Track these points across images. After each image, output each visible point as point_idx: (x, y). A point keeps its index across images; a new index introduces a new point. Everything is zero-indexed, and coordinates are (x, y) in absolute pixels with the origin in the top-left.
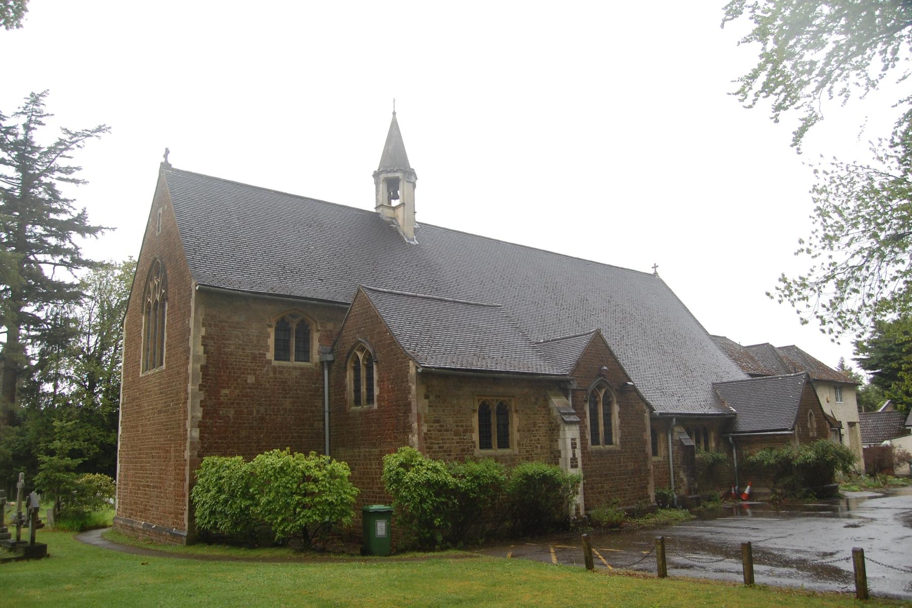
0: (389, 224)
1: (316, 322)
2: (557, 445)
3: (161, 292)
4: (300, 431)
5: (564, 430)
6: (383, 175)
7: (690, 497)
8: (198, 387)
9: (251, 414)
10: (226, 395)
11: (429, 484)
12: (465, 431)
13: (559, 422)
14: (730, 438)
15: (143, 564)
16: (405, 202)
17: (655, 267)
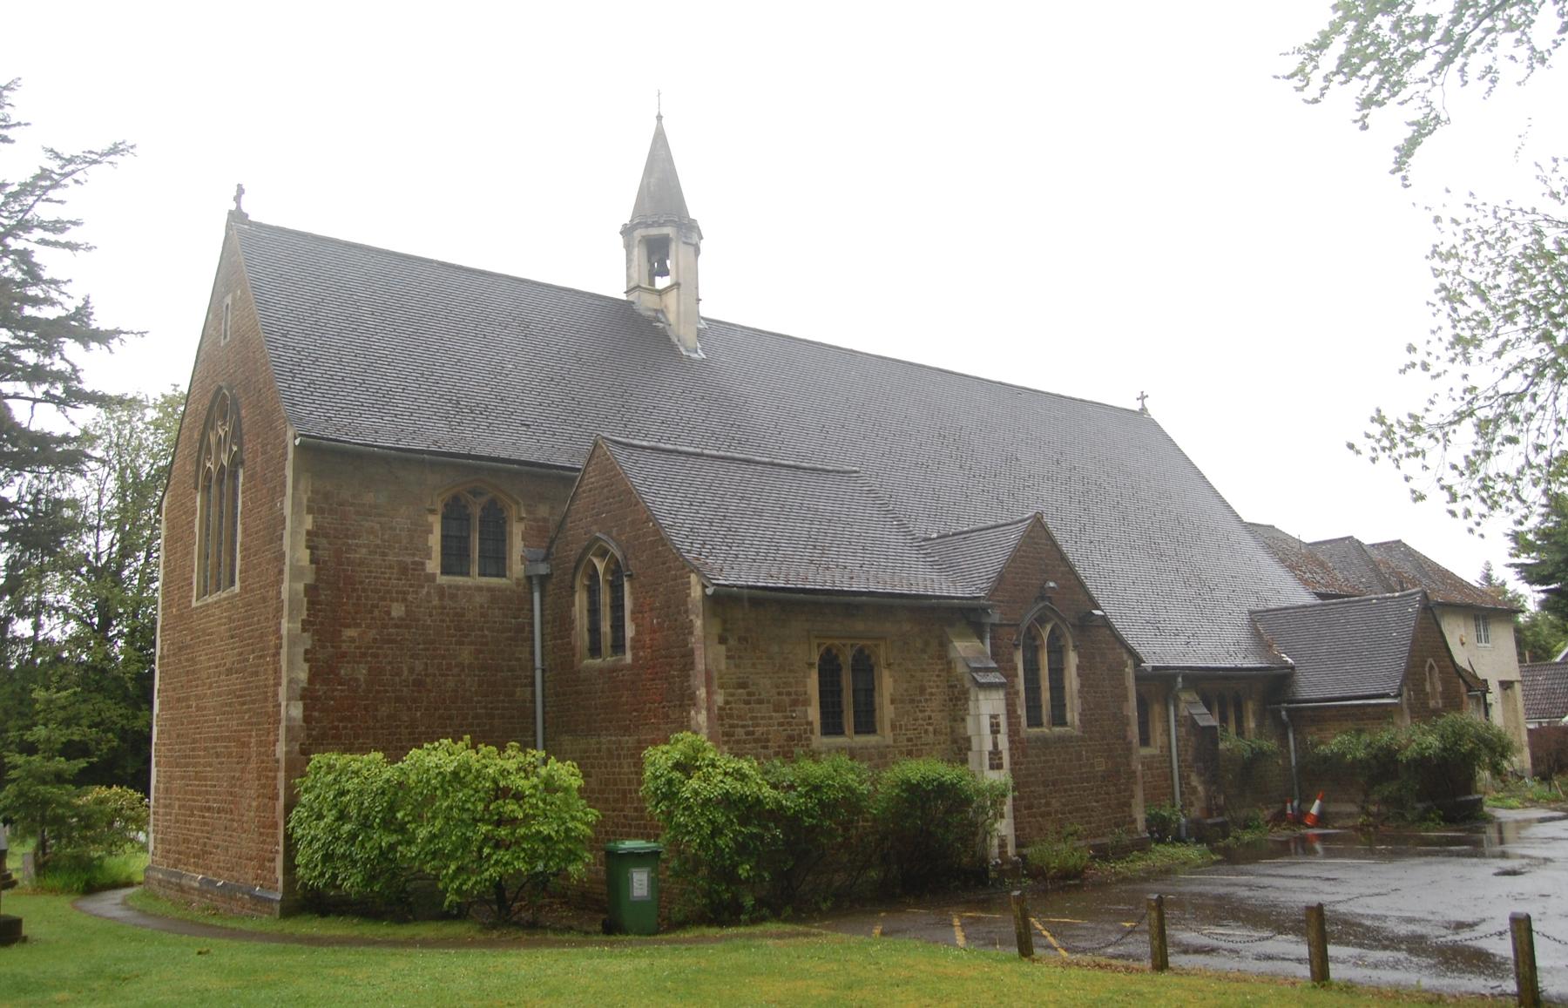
0: (651, 322)
1: (518, 503)
2: (965, 728)
3: (231, 449)
4: (490, 706)
5: (977, 700)
7: (1209, 821)
8: (300, 626)
9: (399, 674)
10: (353, 640)
12: (795, 703)
13: (968, 685)
14: (1284, 713)
15: (200, 953)
16: (681, 281)
17: (1143, 397)
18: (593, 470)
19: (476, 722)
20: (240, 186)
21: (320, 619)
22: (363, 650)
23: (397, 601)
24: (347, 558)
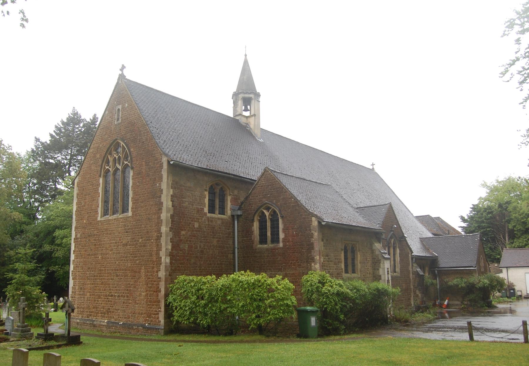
0: (245, 127)
1: (229, 189)
2: (379, 272)
3: (123, 163)
4: (222, 260)
5: (384, 263)
6: (241, 95)
7: (422, 306)
8: (169, 229)
9: (197, 248)
11: (338, 294)
13: (380, 258)
14: (436, 271)
15: (180, 346)
16: (256, 114)
17: (373, 165)
18: (263, 179)
19: (218, 266)
20: (123, 65)
21: (175, 227)
22: (187, 239)
23: (196, 222)
24: (183, 206)
